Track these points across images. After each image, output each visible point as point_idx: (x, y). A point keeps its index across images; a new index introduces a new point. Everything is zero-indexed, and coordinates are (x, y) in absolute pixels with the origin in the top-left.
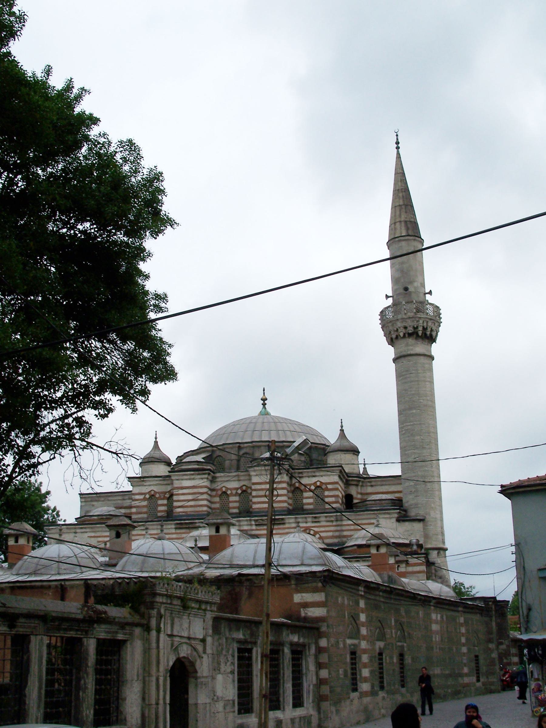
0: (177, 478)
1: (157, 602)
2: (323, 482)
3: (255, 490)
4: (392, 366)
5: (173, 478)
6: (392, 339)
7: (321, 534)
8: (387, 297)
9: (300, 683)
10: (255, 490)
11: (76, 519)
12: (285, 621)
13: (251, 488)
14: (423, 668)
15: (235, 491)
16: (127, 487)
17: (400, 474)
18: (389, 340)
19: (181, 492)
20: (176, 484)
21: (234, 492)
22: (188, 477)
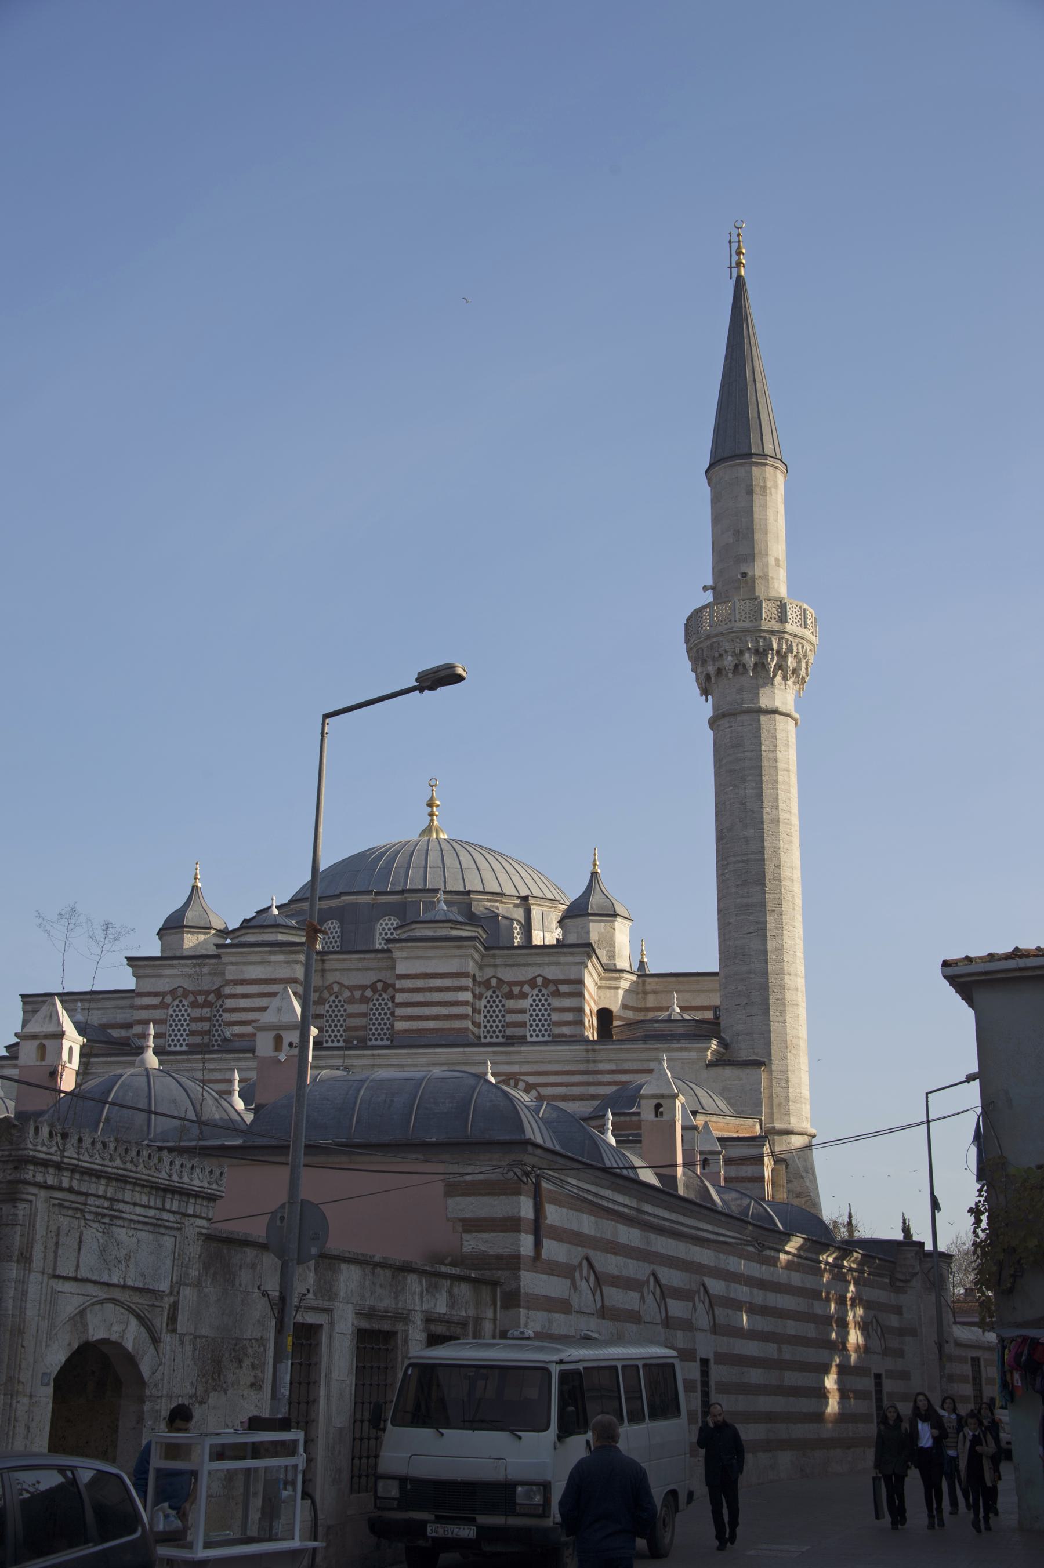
0: (233, 959)
1: (28, 1183)
2: (550, 977)
3: (402, 990)
4: (708, 736)
5: (225, 959)
6: (708, 677)
7: (539, 1089)
8: (705, 588)
9: (564, 1376)
10: (402, 990)
11: (7, 1047)
12: (104, 1116)
13: (393, 986)
14: (919, 1394)
15: (360, 992)
16: (127, 981)
17: (717, 970)
18: (702, 679)
19: (240, 990)
20: (231, 972)
21: (357, 994)
22: (258, 959)
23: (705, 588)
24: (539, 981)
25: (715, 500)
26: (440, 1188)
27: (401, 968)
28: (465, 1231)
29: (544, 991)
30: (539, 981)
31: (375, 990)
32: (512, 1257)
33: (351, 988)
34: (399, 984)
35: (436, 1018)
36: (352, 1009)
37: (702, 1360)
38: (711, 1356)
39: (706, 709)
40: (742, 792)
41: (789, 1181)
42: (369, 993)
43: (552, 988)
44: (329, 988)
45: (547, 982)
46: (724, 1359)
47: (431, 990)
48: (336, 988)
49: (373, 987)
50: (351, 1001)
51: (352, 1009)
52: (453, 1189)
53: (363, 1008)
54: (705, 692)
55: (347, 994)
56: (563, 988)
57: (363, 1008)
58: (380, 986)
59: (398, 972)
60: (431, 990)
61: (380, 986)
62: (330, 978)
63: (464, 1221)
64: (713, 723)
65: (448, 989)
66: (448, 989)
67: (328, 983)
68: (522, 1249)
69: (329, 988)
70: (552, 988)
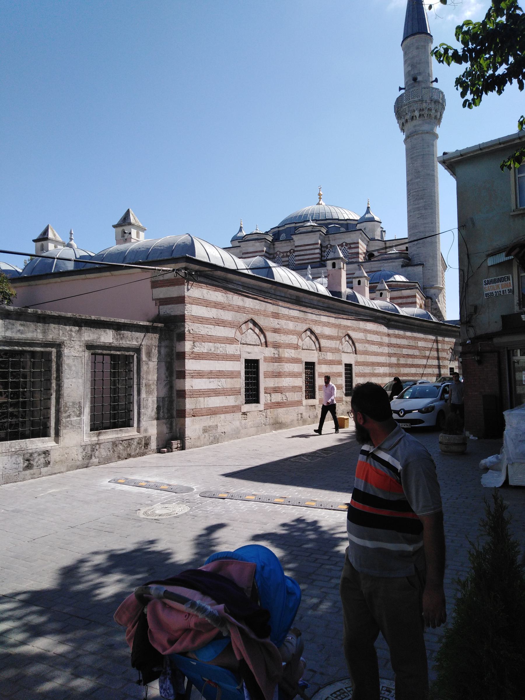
8: (400, 89)
21: (285, 254)
23: (400, 89)
24: (344, 244)
25: (405, 54)
26: (149, 285)
27: (297, 244)
28: (160, 305)
29: (346, 247)
30: (344, 244)
31: (291, 253)
32: (181, 316)
33: (283, 253)
34: (296, 249)
35: (308, 259)
36: (283, 259)
37: (346, 365)
38: (353, 362)
39: (403, 136)
40: (415, 165)
41: (432, 305)
42: (288, 254)
43: (349, 246)
44: (276, 253)
45: (347, 244)
46: (358, 363)
47: (306, 250)
48: (278, 253)
49: (290, 251)
50: (283, 257)
51: (283, 259)
52: (155, 284)
53: (287, 259)
54: (403, 130)
55: (282, 255)
56: (352, 246)
57: (287, 259)
58: (292, 251)
59: (296, 245)
60: (306, 250)
61: (292, 251)
62: (276, 250)
63: (160, 299)
64: (405, 141)
65: (312, 249)
66: (312, 249)
67: (276, 251)
68: (186, 312)
69: (276, 253)
70: (349, 246)
